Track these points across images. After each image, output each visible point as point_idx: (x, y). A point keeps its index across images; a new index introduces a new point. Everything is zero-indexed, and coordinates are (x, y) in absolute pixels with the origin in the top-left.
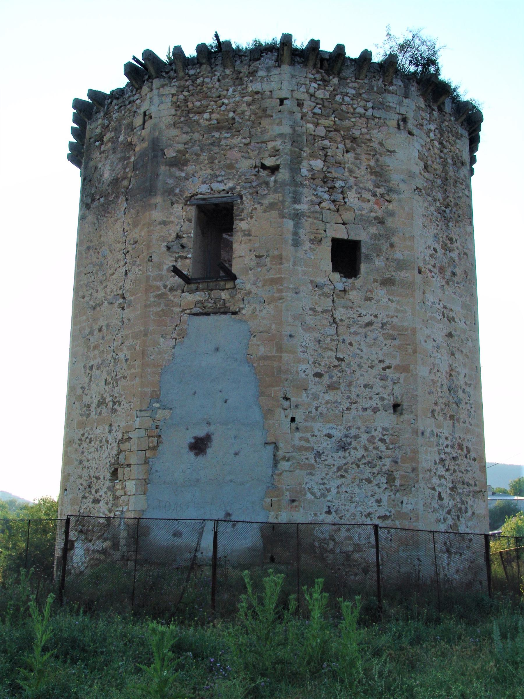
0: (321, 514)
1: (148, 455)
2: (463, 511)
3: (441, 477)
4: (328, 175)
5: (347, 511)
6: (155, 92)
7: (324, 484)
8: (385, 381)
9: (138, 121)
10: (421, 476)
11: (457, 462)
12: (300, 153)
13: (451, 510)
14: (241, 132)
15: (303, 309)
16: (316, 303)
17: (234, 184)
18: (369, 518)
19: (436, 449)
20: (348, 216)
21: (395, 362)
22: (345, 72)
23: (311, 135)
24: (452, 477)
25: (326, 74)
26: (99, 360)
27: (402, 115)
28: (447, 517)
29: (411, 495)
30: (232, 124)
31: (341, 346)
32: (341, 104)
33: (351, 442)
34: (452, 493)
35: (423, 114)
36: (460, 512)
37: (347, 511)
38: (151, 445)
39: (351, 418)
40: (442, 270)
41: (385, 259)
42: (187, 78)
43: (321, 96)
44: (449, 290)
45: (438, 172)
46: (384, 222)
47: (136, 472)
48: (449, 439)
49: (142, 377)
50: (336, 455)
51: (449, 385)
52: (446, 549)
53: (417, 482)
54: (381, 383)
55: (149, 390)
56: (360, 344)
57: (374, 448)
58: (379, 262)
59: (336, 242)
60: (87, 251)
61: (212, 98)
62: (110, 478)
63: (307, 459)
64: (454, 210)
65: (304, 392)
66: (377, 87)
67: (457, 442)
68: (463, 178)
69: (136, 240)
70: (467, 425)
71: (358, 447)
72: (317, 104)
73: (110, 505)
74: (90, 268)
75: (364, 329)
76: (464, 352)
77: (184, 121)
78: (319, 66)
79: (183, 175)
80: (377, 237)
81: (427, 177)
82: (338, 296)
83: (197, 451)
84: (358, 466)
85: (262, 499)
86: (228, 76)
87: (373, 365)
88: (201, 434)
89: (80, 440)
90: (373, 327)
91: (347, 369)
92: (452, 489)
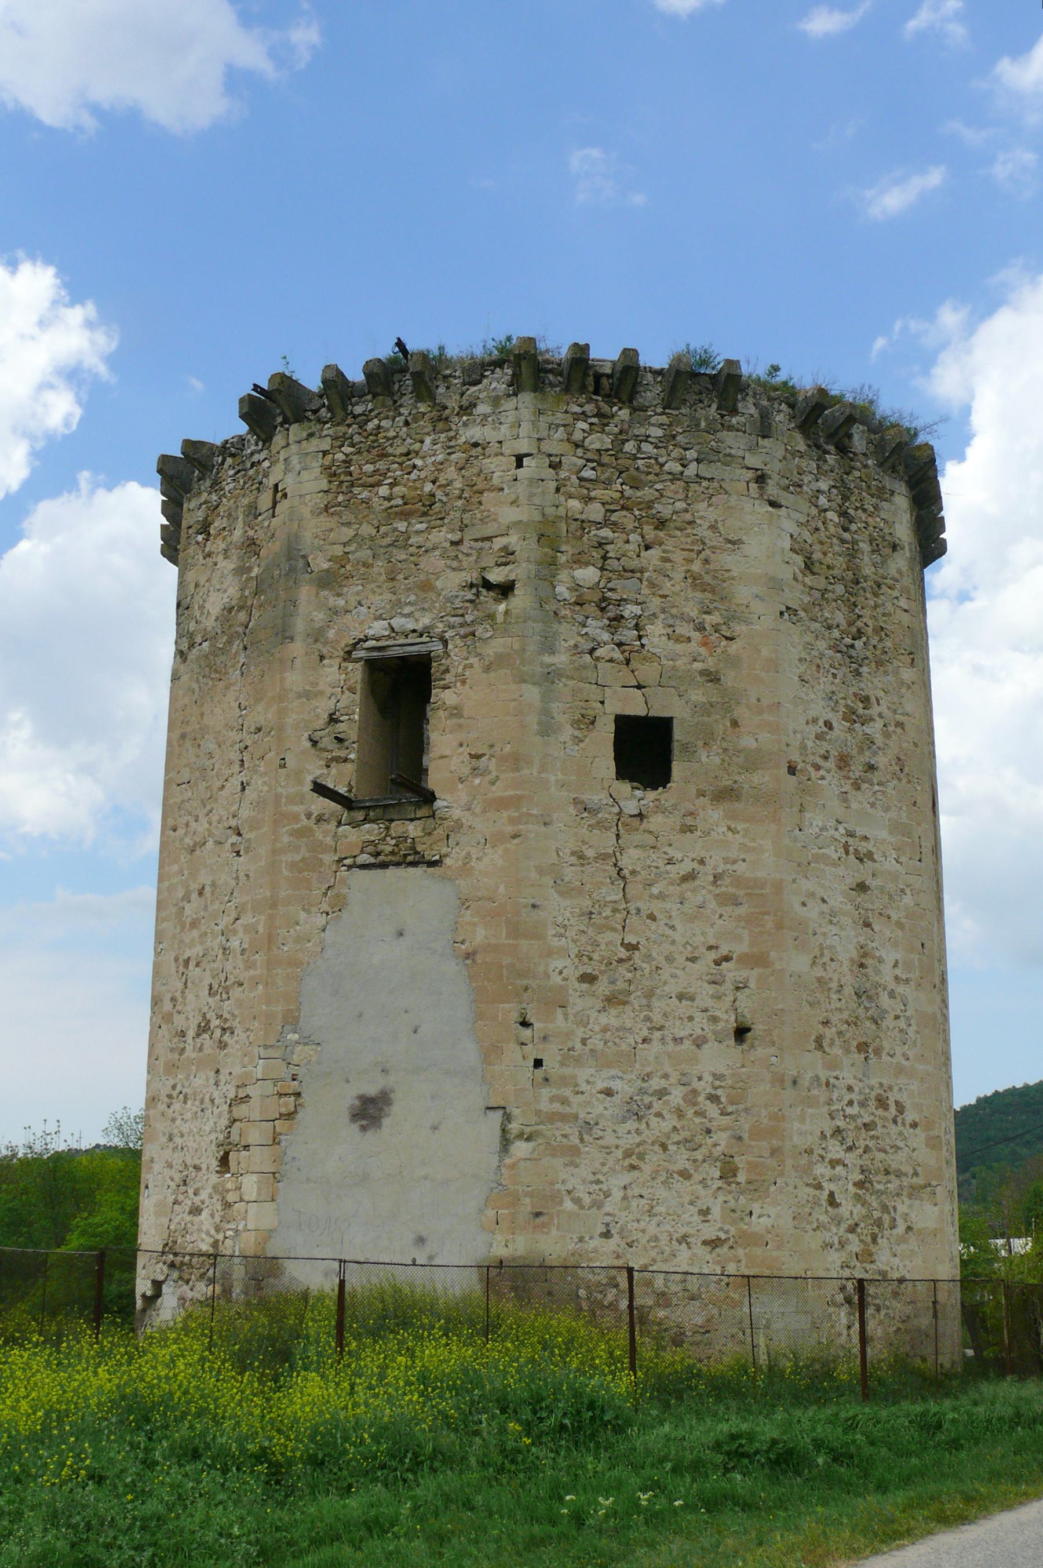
0: (591, 1238)
1: (278, 1130)
2: (886, 1226)
3: (834, 1163)
4: (609, 594)
5: (643, 1231)
6: (294, 448)
7: (598, 1182)
8: (720, 985)
9: (265, 500)
10: (789, 1162)
11: (872, 1133)
12: (555, 558)
13: (857, 1225)
14: (446, 521)
15: (558, 855)
16: (583, 841)
17: (433, 619)
18: (684, 1244)
19: (825, 1110)
20: (647, 672)
21: (741, 948)
22: (642, 396)
23: (576, 520)
24: (860, 1162)
25: (606, 403)
26: (198, 950)
27: (757, 470)
28: (848, 1239)
29: (768, 1200)
30: (430, 506)
31: (633, 921)
32: (635, 458)
33: (651, 1103)
34: (860, 1192)
35: (804, 464)
36: (879, 1226)
37: (643, 1231)
38: (283, 1110)
39: (651, 1059)
40: (844, 762)
41: (720, 751)
42: (349, 421)
43: (597, 446)
44: (859, 801)
45: (836, 572)
46: (719, 680)
47: (258, 1158)
48: (856, 1089)
49: (267, 984)
50: (622, 1129)
51: (857, 986)
52: (845, 1298)
53: (782, 1174)
54: (711, 989)
55: (280, 1008)
56: (670, 917)
57: (695, 1112)
58: (709, 758)
59: (626, 727)
60: (181, 742)
61: (395, 456)
62: (218, 1169)
63: (565, 1136)
64: (874, 641)
65: (559, 1011)
66: (706, 420)
67: (873, 1094)
68: (897, 576)
69: (258, 726)
70: (899, 1059)
71: (664, 1113)
72: (588, 460)
73: (217, 1219)
74: (186, 775)
75: (678, 888)
76: (894, 917)
77: (344, 501)
78: (591, 389)
79: (341, 602)
80: (707, 708)
81: (809, 583)
82: (625, 825)
83: (364, 1122)
84: (664, 1147)
85: (481, 1211)
86: (424, 414)
87: (696, 955)
88: (372, 1090)
89: (170, 1096)
90: (697, 883)
91: (644, 965)
92: (860, 1185)
